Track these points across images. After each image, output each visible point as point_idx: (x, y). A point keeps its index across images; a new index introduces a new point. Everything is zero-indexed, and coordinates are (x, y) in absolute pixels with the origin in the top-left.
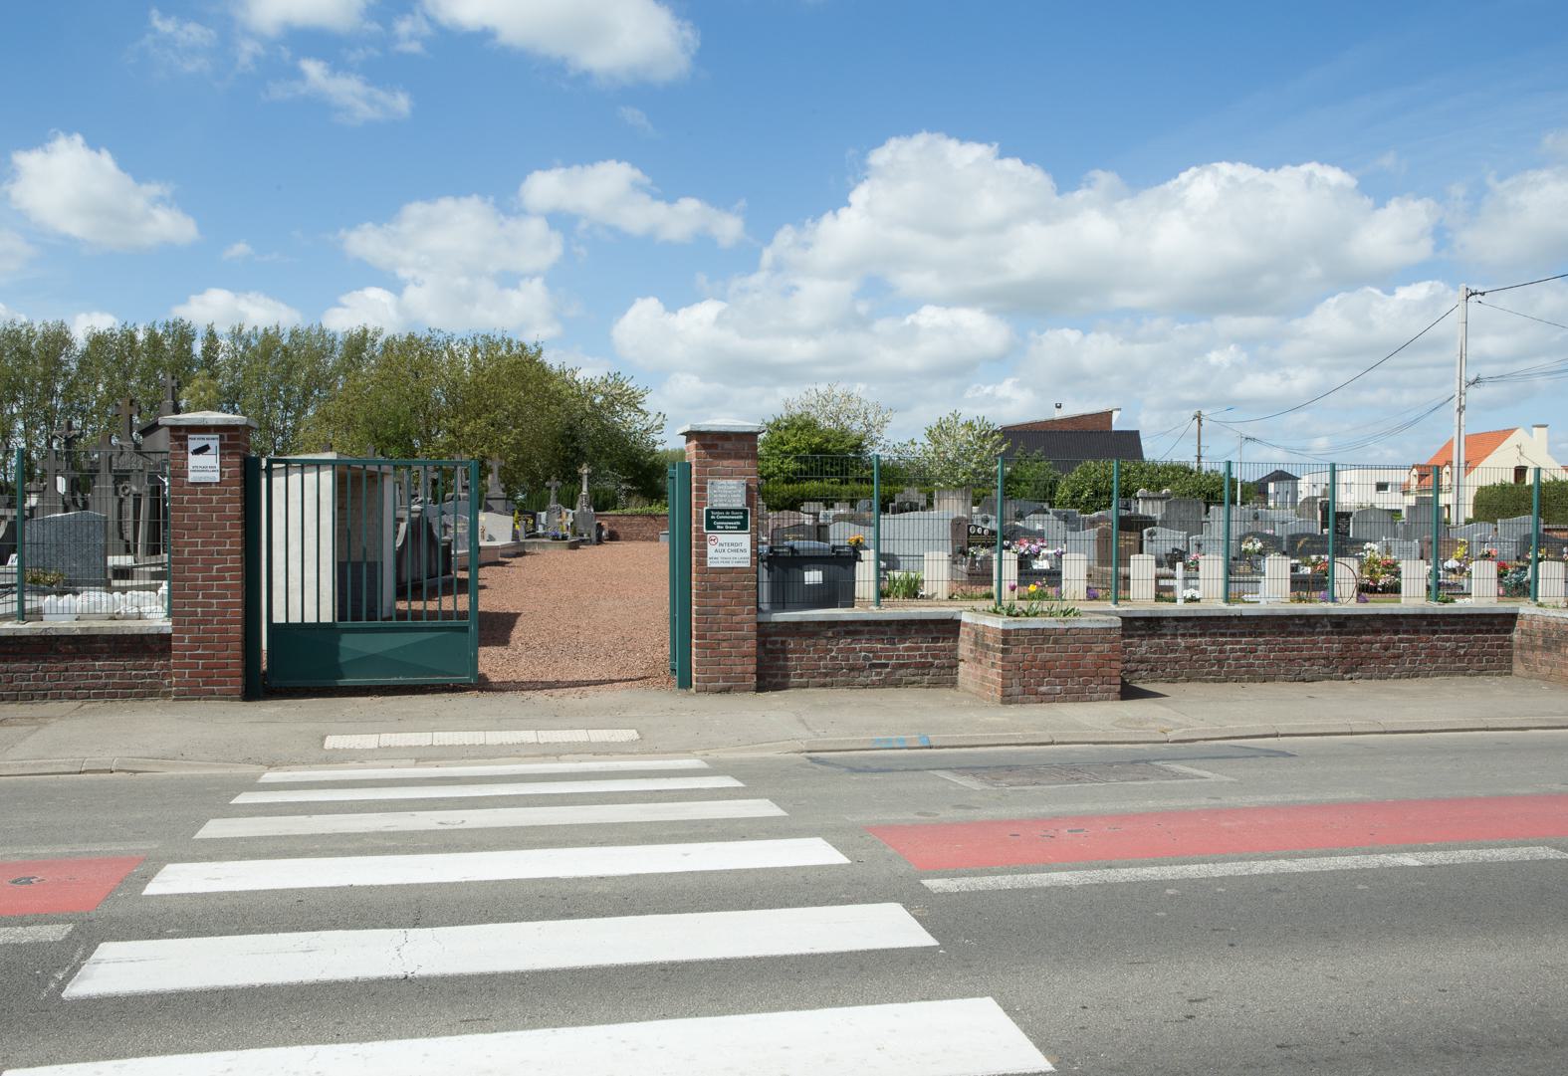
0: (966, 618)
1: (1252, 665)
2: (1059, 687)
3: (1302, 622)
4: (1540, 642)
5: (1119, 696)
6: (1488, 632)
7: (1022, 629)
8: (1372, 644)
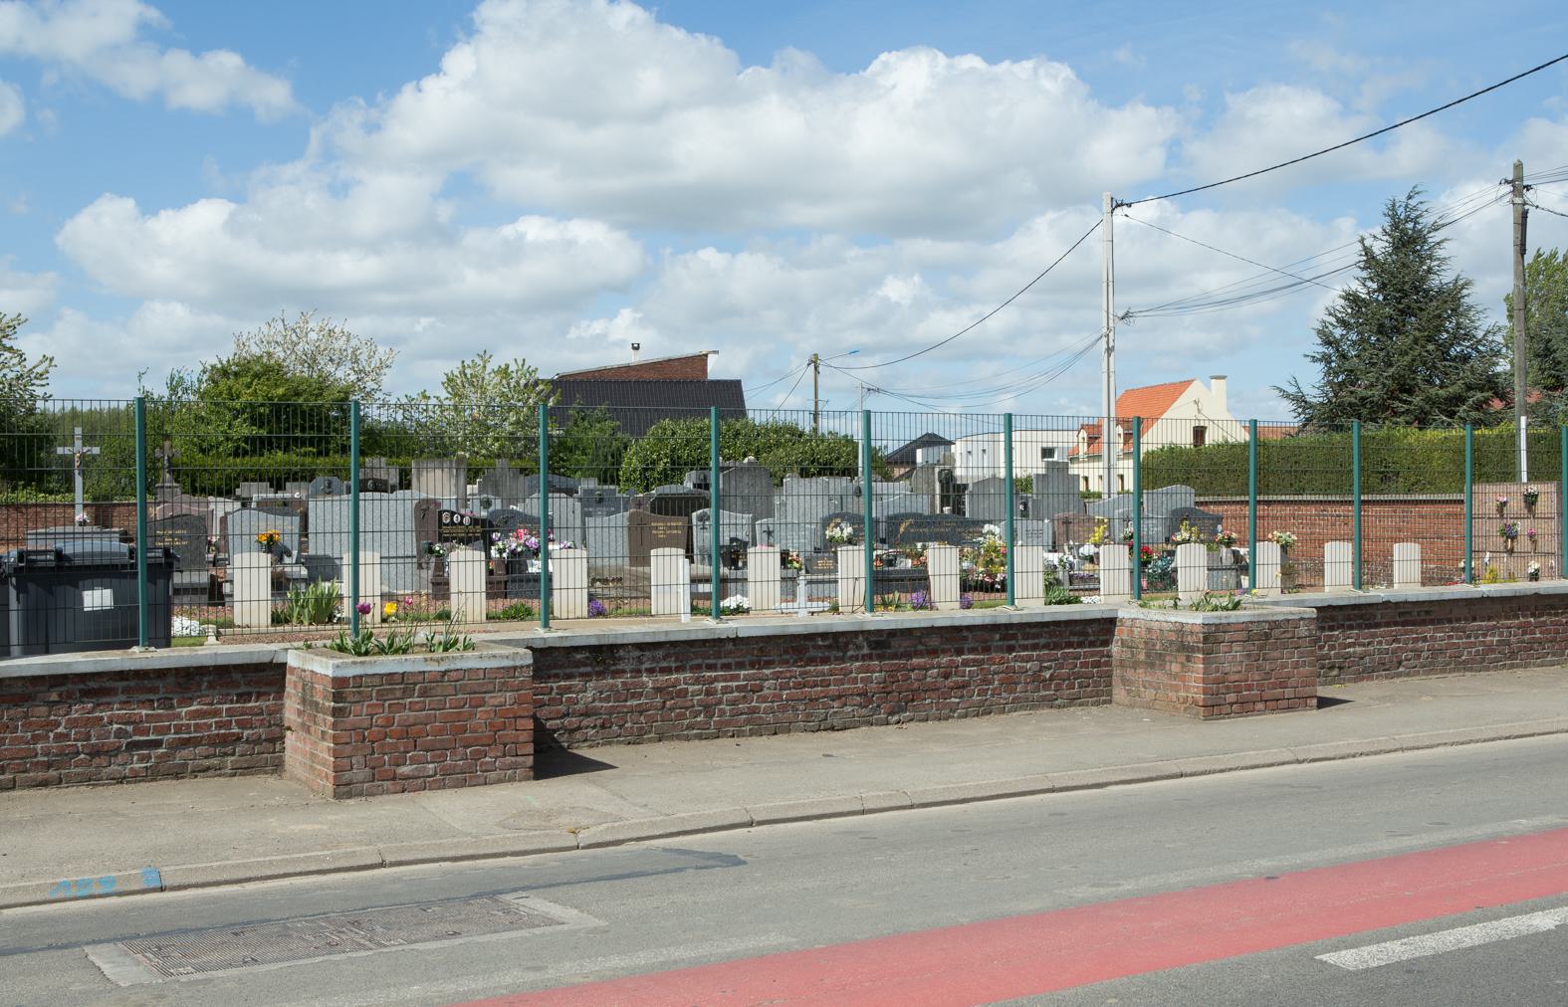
0: (293, 659)
1: (754, 711)
2: (431, 766)
3: (827, 643)
4: (1142, 657)
5: (532, 774)
6: (1081, 645)
7: (367, 675)
8: (927, 670)
